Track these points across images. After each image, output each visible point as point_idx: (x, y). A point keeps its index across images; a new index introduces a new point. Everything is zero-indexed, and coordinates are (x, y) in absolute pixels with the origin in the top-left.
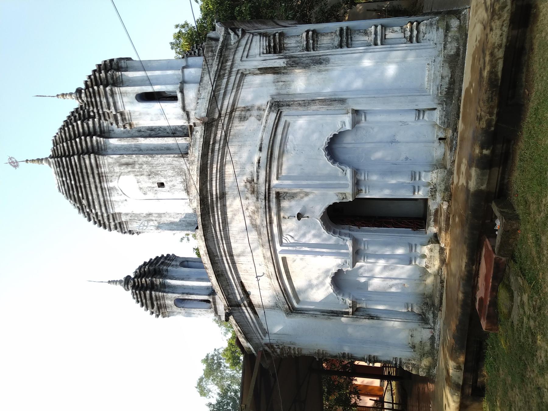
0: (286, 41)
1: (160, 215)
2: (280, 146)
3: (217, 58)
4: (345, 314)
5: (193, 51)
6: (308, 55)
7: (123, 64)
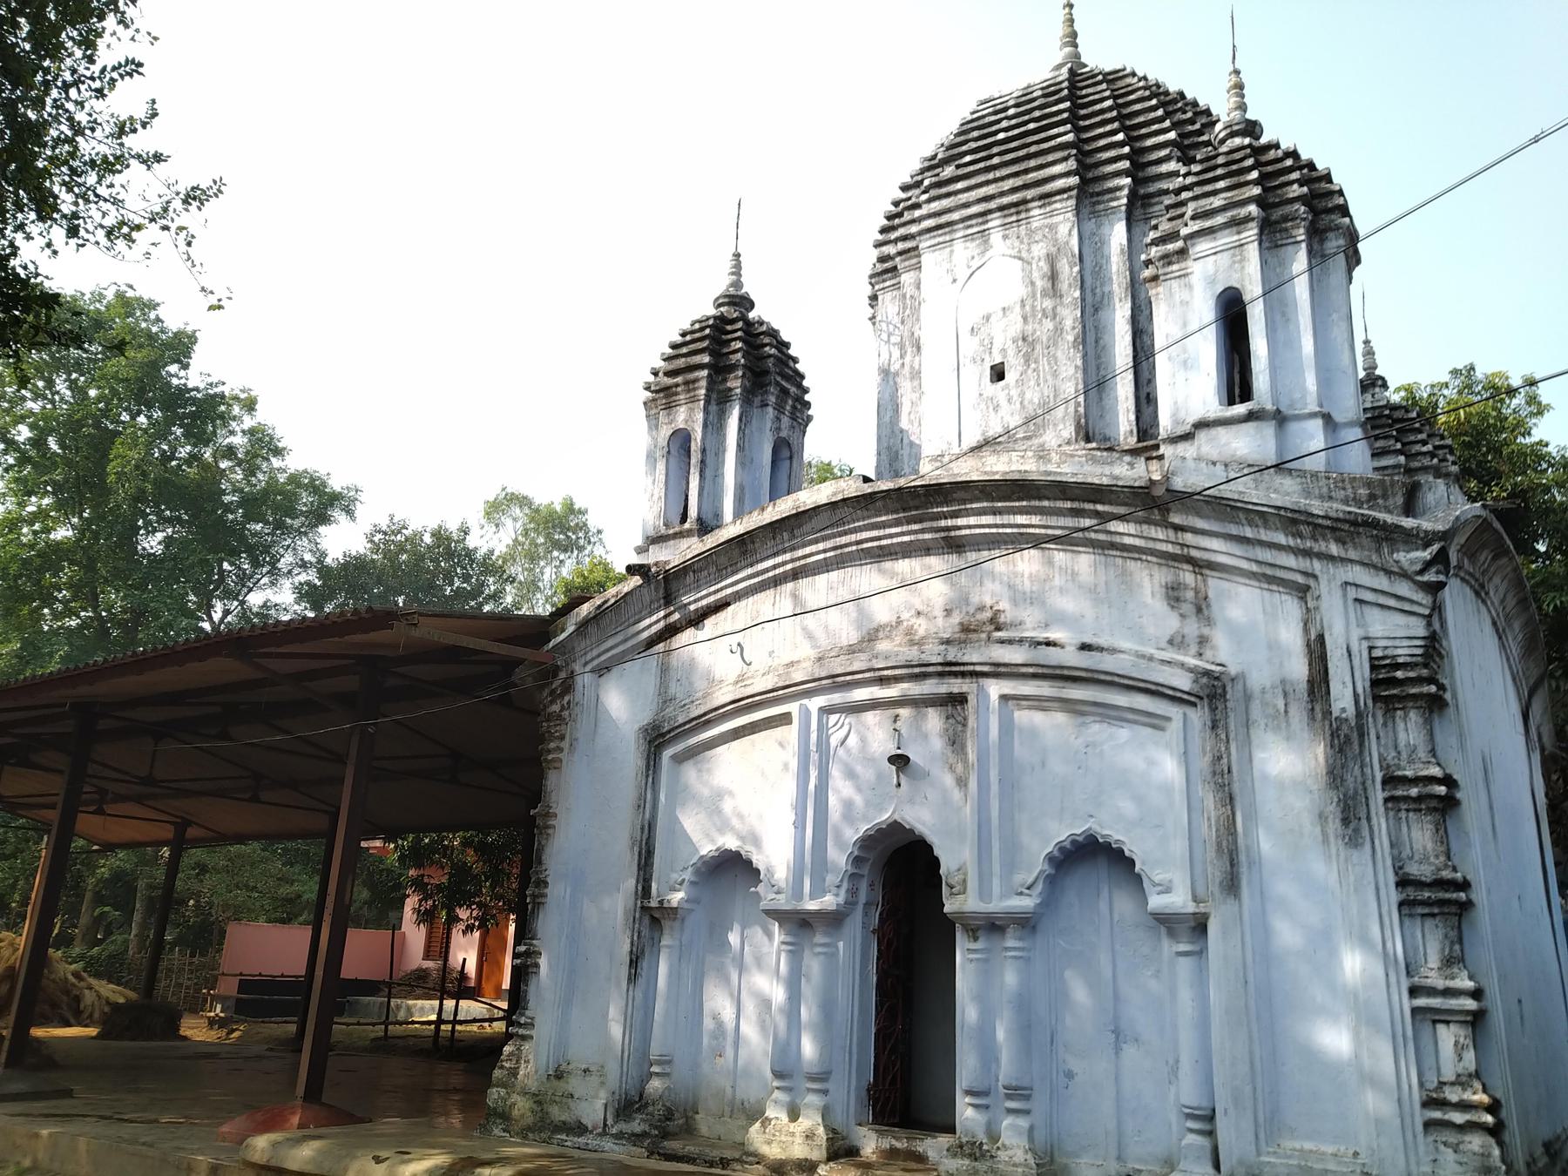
0: (1413, 715)
1: (916, 375)
2: (1095, 704)
3: (1349, 513)
4: (643, 888)
5: (1429, 436)
6: (1369, 782)
7: (1335, 243)
